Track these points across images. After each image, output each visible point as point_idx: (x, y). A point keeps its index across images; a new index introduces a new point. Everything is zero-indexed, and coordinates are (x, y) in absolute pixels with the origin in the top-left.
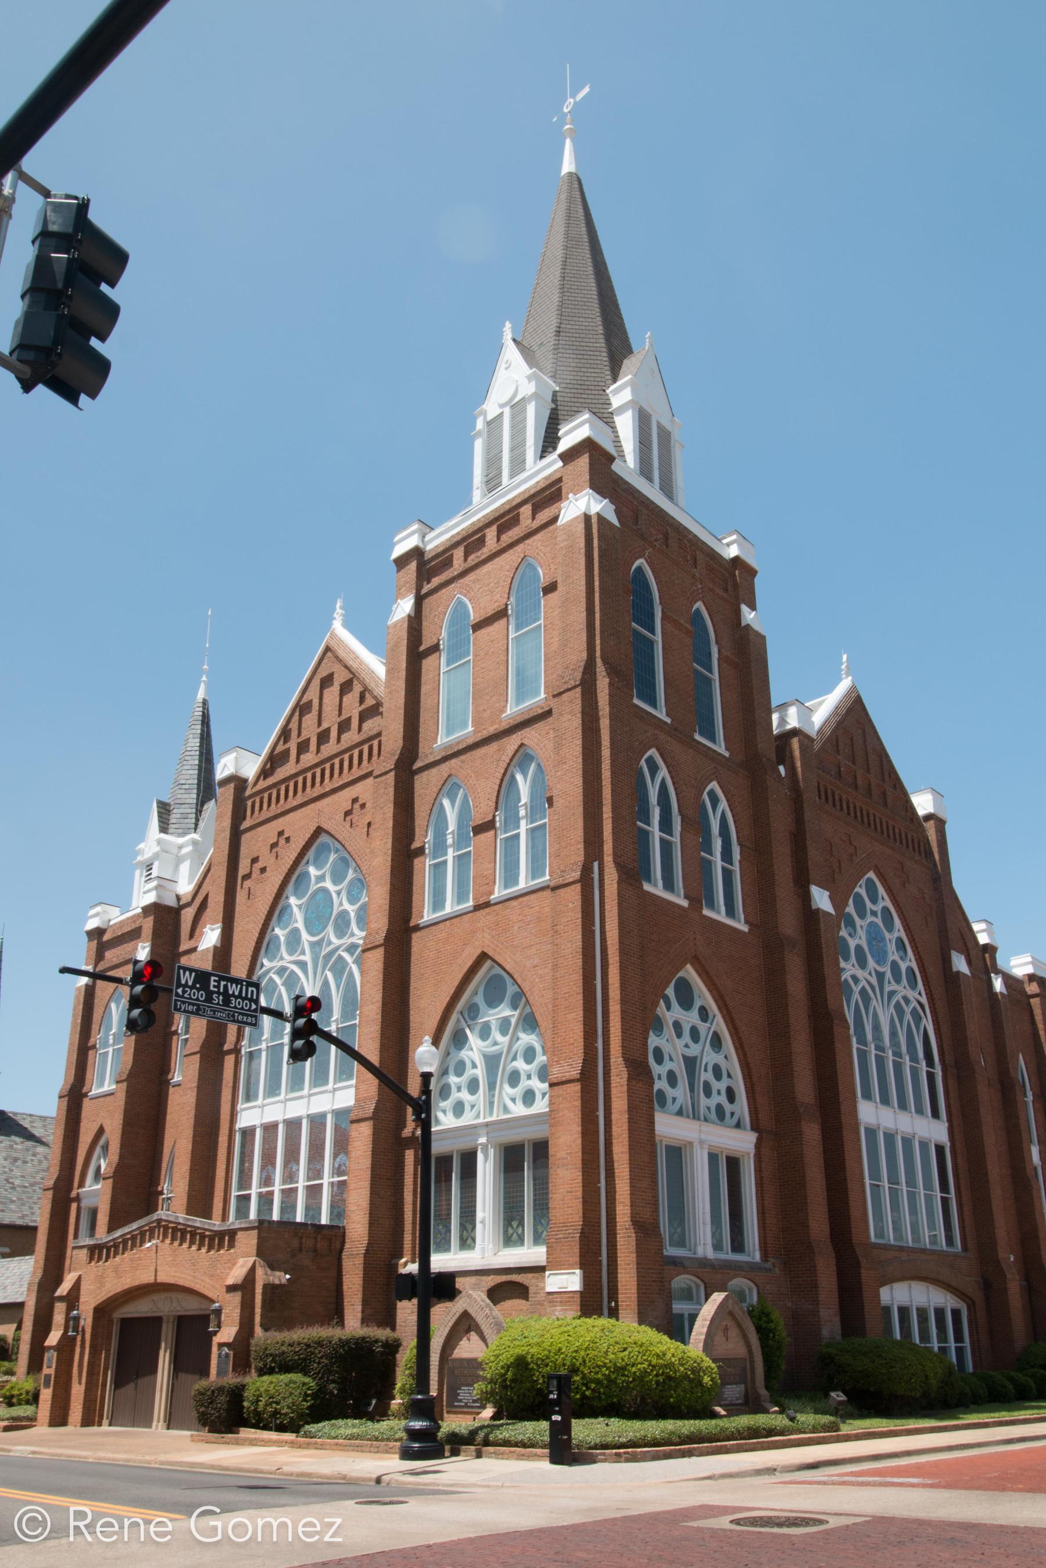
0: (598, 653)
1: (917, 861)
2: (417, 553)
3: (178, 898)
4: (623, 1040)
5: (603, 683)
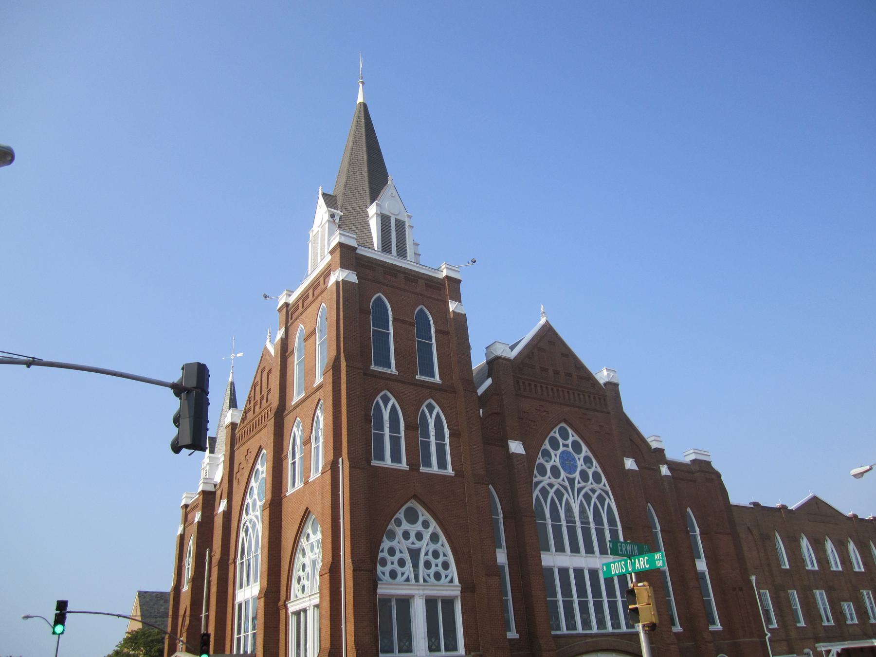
0: (342, 351)
1: (597, 411)
2: (286, 305)
3: (215, 486)
4: (352, 550)
5: (343, 364)
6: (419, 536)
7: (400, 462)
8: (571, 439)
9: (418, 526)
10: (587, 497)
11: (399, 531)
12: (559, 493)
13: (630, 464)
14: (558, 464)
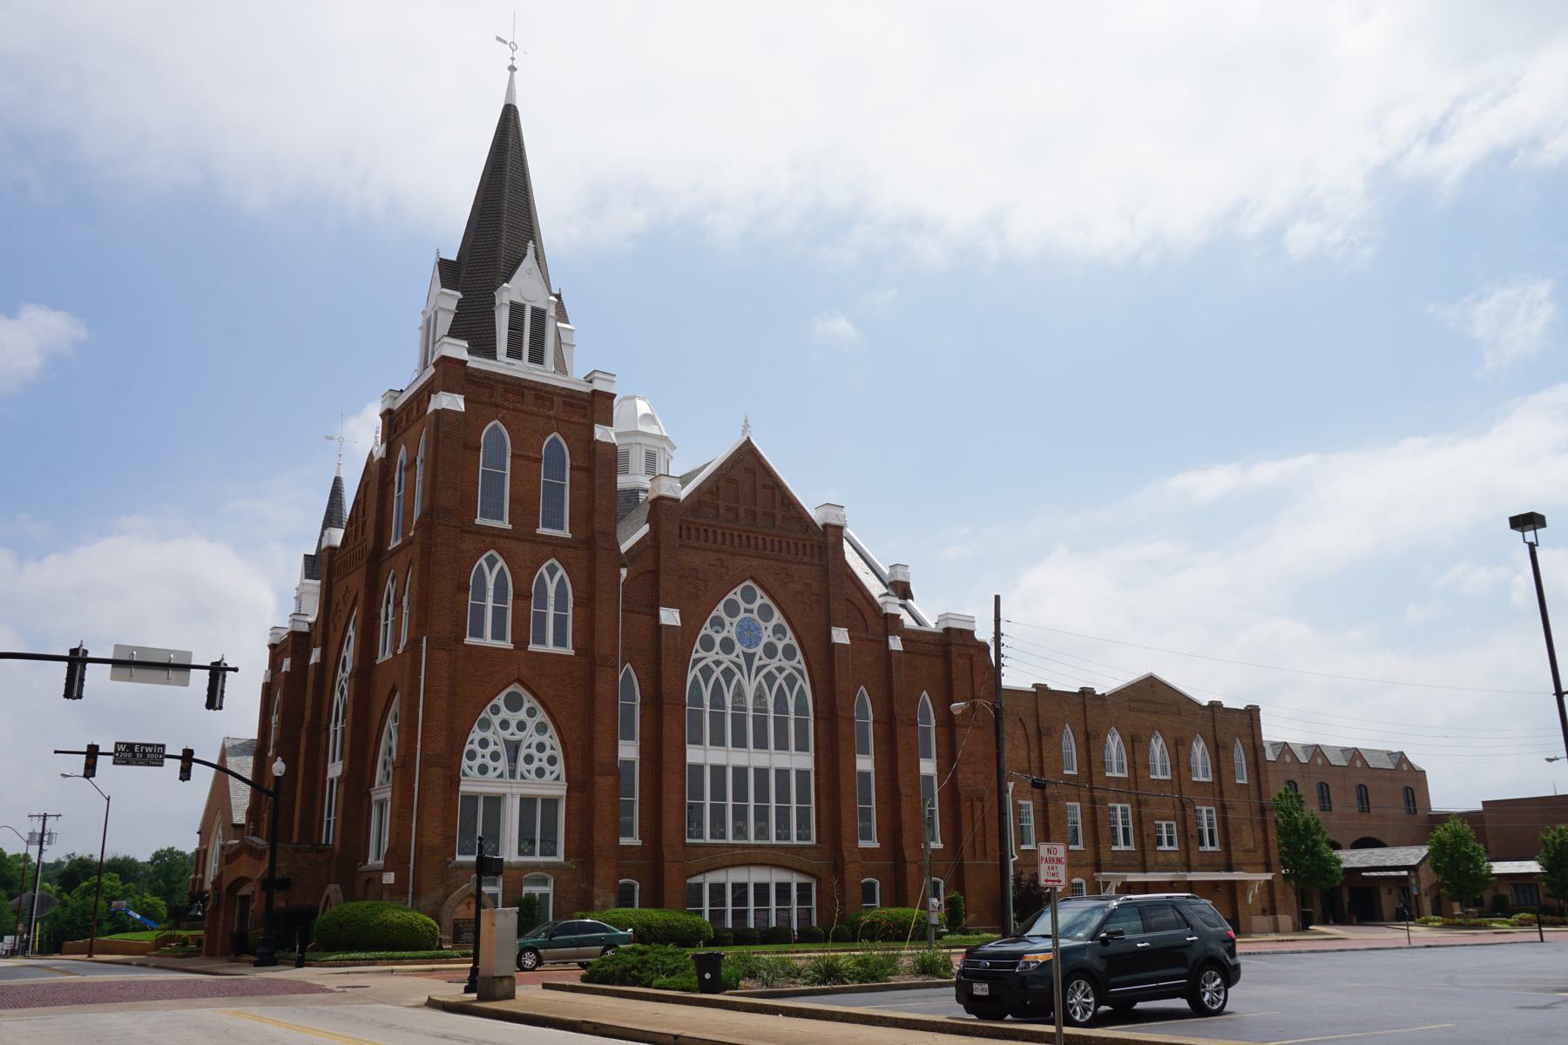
10: (770, 678)
12: (728, 674)
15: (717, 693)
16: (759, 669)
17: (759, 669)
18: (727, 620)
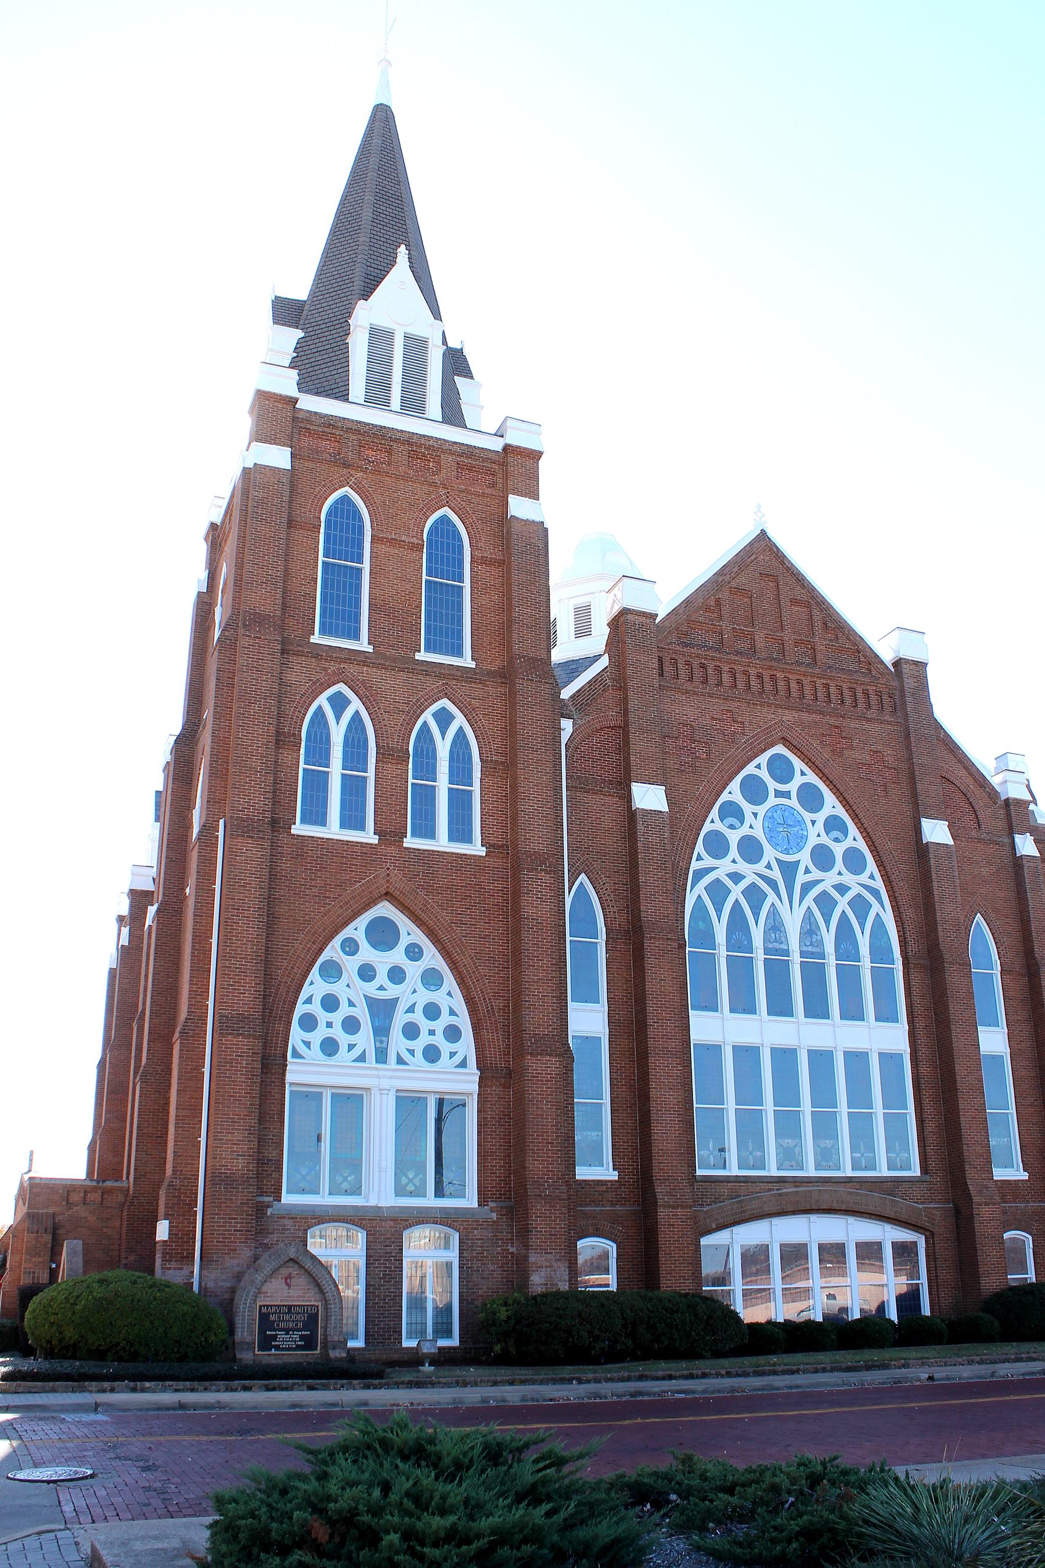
6: (397, 975)
7: (468, 839)
8: (797, 781)
9: (397, 956)
10: (825, 902)
11: (351, 965)
12: (755, 896)
13: (936, 832)
14: (759, 833)
15: (738, 924)
16: (806, 888)
17: (806, 888)
18: (747, 808)
